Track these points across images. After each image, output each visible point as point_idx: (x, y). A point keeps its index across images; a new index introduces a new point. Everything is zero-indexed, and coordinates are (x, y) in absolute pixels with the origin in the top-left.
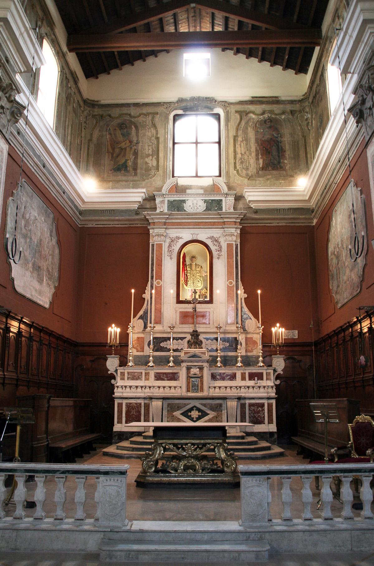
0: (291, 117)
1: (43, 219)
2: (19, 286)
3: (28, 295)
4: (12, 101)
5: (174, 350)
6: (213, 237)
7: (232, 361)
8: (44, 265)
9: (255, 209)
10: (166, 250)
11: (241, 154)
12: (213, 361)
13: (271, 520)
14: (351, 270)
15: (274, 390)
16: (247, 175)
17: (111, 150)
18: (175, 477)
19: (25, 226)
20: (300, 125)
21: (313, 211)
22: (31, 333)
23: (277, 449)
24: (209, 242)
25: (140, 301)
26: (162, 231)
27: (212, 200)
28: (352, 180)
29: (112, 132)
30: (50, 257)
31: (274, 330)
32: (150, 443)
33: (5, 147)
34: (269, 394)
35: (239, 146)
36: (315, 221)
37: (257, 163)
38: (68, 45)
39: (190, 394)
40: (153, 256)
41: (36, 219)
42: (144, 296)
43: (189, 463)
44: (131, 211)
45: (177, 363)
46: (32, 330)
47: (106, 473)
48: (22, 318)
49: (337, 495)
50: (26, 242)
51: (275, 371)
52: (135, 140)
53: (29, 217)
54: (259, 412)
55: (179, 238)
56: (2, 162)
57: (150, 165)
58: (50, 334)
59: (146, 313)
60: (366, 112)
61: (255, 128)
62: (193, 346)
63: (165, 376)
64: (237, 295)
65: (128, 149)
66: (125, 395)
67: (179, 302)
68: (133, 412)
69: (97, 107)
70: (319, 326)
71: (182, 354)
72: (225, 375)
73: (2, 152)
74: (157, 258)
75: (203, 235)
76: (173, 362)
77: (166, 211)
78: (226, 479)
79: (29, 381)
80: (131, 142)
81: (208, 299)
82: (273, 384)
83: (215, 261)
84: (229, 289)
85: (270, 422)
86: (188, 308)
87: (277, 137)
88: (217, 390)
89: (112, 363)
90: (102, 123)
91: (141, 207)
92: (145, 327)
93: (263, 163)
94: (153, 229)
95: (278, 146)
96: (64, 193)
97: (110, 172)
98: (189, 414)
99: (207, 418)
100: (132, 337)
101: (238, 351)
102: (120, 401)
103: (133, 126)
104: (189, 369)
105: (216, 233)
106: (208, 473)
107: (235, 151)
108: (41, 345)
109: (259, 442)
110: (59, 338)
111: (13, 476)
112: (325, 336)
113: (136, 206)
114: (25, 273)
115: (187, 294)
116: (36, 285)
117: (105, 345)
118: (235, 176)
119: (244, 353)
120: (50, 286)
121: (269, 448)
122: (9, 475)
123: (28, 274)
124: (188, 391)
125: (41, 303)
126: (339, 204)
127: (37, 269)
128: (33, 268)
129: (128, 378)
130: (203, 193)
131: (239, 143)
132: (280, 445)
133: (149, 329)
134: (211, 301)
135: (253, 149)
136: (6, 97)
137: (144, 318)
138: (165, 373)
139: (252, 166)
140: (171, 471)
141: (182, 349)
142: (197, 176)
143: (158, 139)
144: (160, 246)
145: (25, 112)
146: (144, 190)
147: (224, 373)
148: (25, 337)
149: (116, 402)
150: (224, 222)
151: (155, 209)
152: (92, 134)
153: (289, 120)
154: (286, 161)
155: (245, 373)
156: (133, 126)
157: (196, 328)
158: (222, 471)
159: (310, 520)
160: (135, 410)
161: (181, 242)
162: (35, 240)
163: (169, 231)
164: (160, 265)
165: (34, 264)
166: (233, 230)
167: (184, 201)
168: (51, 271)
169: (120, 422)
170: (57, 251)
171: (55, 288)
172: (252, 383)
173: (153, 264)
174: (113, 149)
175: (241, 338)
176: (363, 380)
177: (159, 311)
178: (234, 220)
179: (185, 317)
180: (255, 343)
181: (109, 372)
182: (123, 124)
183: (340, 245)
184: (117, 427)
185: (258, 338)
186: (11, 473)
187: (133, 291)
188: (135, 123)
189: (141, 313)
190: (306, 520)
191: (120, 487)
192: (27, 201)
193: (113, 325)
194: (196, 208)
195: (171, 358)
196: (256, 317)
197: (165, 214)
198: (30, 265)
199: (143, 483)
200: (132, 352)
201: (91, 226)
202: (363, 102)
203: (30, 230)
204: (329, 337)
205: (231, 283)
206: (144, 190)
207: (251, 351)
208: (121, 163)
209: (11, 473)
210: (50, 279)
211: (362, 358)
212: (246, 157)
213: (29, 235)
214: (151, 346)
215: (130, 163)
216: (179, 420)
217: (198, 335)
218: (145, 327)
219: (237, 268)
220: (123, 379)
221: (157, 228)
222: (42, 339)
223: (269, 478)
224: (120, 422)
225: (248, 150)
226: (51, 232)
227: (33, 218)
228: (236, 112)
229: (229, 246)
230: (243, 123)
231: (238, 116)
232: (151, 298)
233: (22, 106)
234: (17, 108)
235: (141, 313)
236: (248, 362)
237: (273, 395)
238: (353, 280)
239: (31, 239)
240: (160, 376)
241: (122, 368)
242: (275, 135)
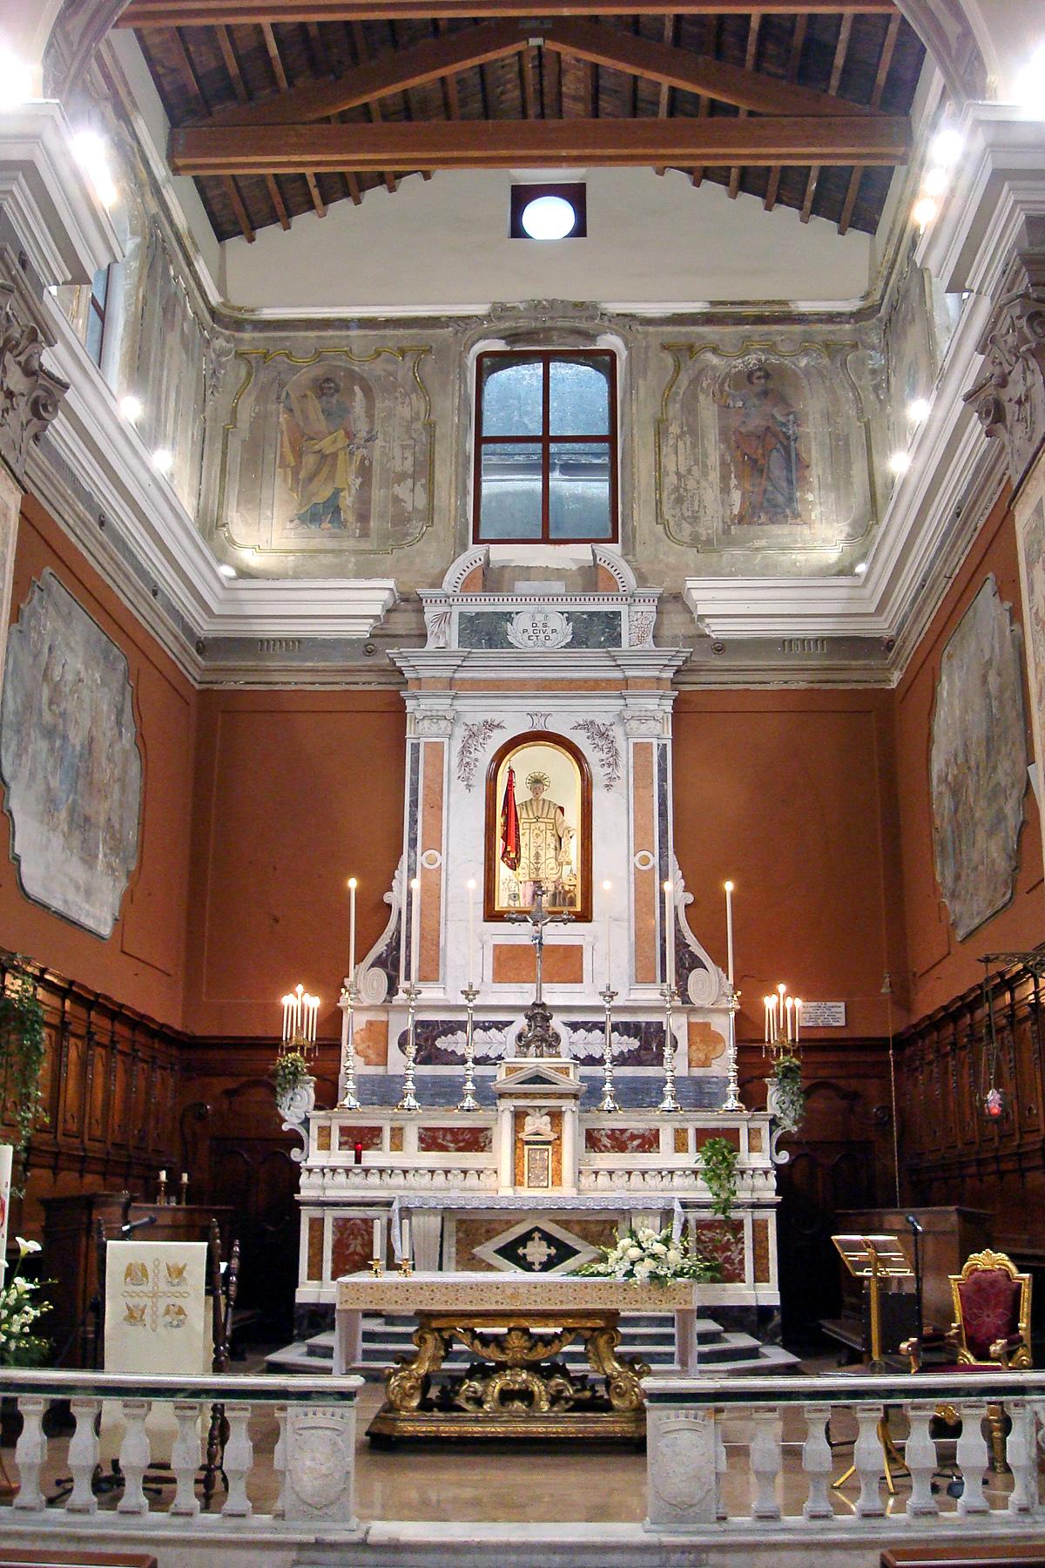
0: (826, 361)
1: (97, 676)
2: (34, 878)
3: (56, 904)
4: (32, 372)
5: (477, 1061)
6: (592, 722)
7: (648, 1092)
8: (101, 810)
9: (718, 641)
10: (455, 761)
11: (678, 473)
12: (590, 1095)
13: (724, 1518)
14: (991, 834)
15: (773, 1182)
17: (291, 459)
18: (477, 1420)
19: (51, 703)
20: (854, 387)
21: (890, 645)
22: (64, 1012)
23: (778, 1355)
24: (580, 739)
25: (377, 912)
26: (441, 705)
27: (591, 614)
28: (990, 575)
29: (296, 406)
30: (117, 787)
31: (770, 1002)
32: (405, 1338)
33: (14, 500)
34: (756, 1195)
35: (670, 450)
36: (896, 677)
38: (171, 156)
39: (13, 1395)
40: (416, 776)
41: (81, 680)
42: (387, 897)
43: (515, 1382)
44: (350, 642)
45: (486, 1098)
46: (68, 1003)
47: (304, 1395)
48: (43, 971)
49: (895, 1454)
50: (52, 750)
51: (774, 1122)
52: (362, 428)
53: (62, 676)
55: (491, 726)
56: (5, 544)
58: (116, 1013)
59: (394, 947)
60: (1011, 410)
61: (720, 397)
62: (532, 1049)
63: (449, 1137)
64: (662, 894)
65: (341, 456)
66: (332, 1194)
67: (492, 915)
68: (356, 1245)
69: (248, 327)
70: (908, 991)
71: (500, 1073)
72: (627, 1134)
73: (5, 516)
74: (426, 787)
76: (476, 1096)
77: (455, 646)
78: (618, 1428)
79: (57, 1154)
80: (350, 435)
82: (768, 1164)
83: (598, 795)
84: (641, 882)
85: (761, 1276)
86: (521, 934)
87: (784, 424)
88: (603, 1180)
89: (296, 1107)
90: (264, 377)
91: (382, 635)
92: (392, 990)
93: (742, 503)
94: (416, 697)
95: (787, 449)
96: (155, 593)
97: (289, 525)
98: (521, 1251)
99: (571, 1263)
100: (354, 1024)
101: (667, 1066)
103: (357, 388)
104: (519, 1116)
105: (602, 710)
106: (568, 1411)
107: (659, 465)
108: (89, 1047)
109: (725, 1335)
110: (138, 1022)
111: (66, 1403)
112: (923, 1020)
113: (363, 629)
114: (49, 840)
116: (78, 871)
117: (273, 1045)
118: (659, 540)
119: (682, 1070)
120: (113, 870)
121: (752, 1353)
122: (53, 1401)
123: (57, 841)
124: (516, 1181)
125: (89, 923)
126: (957, 637)
127: (81, 823)
128: (71, 822)
129: (341, 1144)
130: (563, 591)
131: (671, 442)
132: (788, 1346)
133: (401, 996)
134: (585, 916)
135: (714, 459)
136: (19, 363)
137: (390, 964)
138: (451, 1130)
140: (465, 1406)
141: (500, 1058)
142: (546, 540)
143: (430, 427)
144: (436, 750)
145: (69, 395)
146: (390, 583)
147: (623, 1131)
148: (47, 1024)
149: (306, 1215)
150: (626, 679)
151: (423, 637)
152: (234, 411)
153: (820, 373)
154: (810, 497)
155: (685, 1130)
156: (357, 388)
157: (540, 1008)
158: (607, 1407)
159: (825, 1517)
160: (359, 1241)
161: (499, 739)
162: (76, 739)
163: (460, 705)
164: (436, 806)
165: (72, 811)
166: (651, 704)
167: (508, 617)
168: (117, 826)
170: (135, 768)
171: (129, 875)
172: (433, 1159)
173: (414, 804)
174: (299, 455)
175: (677, 1025)
176: (1020, 1155)
177: (432, 942)
178: (656, 674)
180: (716, 1039)
181: (285, 1127)
182: (328, 380)
183: (960, 759)
184: (307, 1292)
185: (724, 1026)
186: (60, 1397)
187: (353, 883)
188: (362, 379)
189: (380, 947)
190: (814, 1517)
191: (339, 1432)
192: (56, 631)
193: (300, 988)
194: (542, 636)
195: (470, 1086)
196: (720, 961)
197: (452, 655)
198: (63, 815)
199: (389, 1437)
200: (353, 1065)
201: (231, 686)
202: (1003, 383)
203: (63, 714)
204: (934, 1023)
205: (645, 861)
206: (390, 583)
207: (705, 1064)
208: (320, 499)
209: (60, 1397)
210: (114, 850)
211: (993, 1097)
212: (691, 484)
213: (61, 727)
214: (412, 1049)
215: (347, 500)
216: (490, 1268)
217: (547, 1019)
218: (392, 990)
219: (663, 815)
221: (428, 697)
222: (68, 1018)
223: (719, 1410)
224: (315, 1274)
225: (696, 463)
226: (120, 712)
227: (70, 677)
228: (664, 347)
229: (641, 750)
230: (684, 380)
231: (669, 360)
232: (409, 904)
233: (58, 381)
234: (47, 390)
235: (380, 947)
236: (699, 1094)
237: (770, 1195)
238: (993, 862)
239: (65, 738)
240: (434, 1138)
241: (322, 1113)
242: (780, 418)
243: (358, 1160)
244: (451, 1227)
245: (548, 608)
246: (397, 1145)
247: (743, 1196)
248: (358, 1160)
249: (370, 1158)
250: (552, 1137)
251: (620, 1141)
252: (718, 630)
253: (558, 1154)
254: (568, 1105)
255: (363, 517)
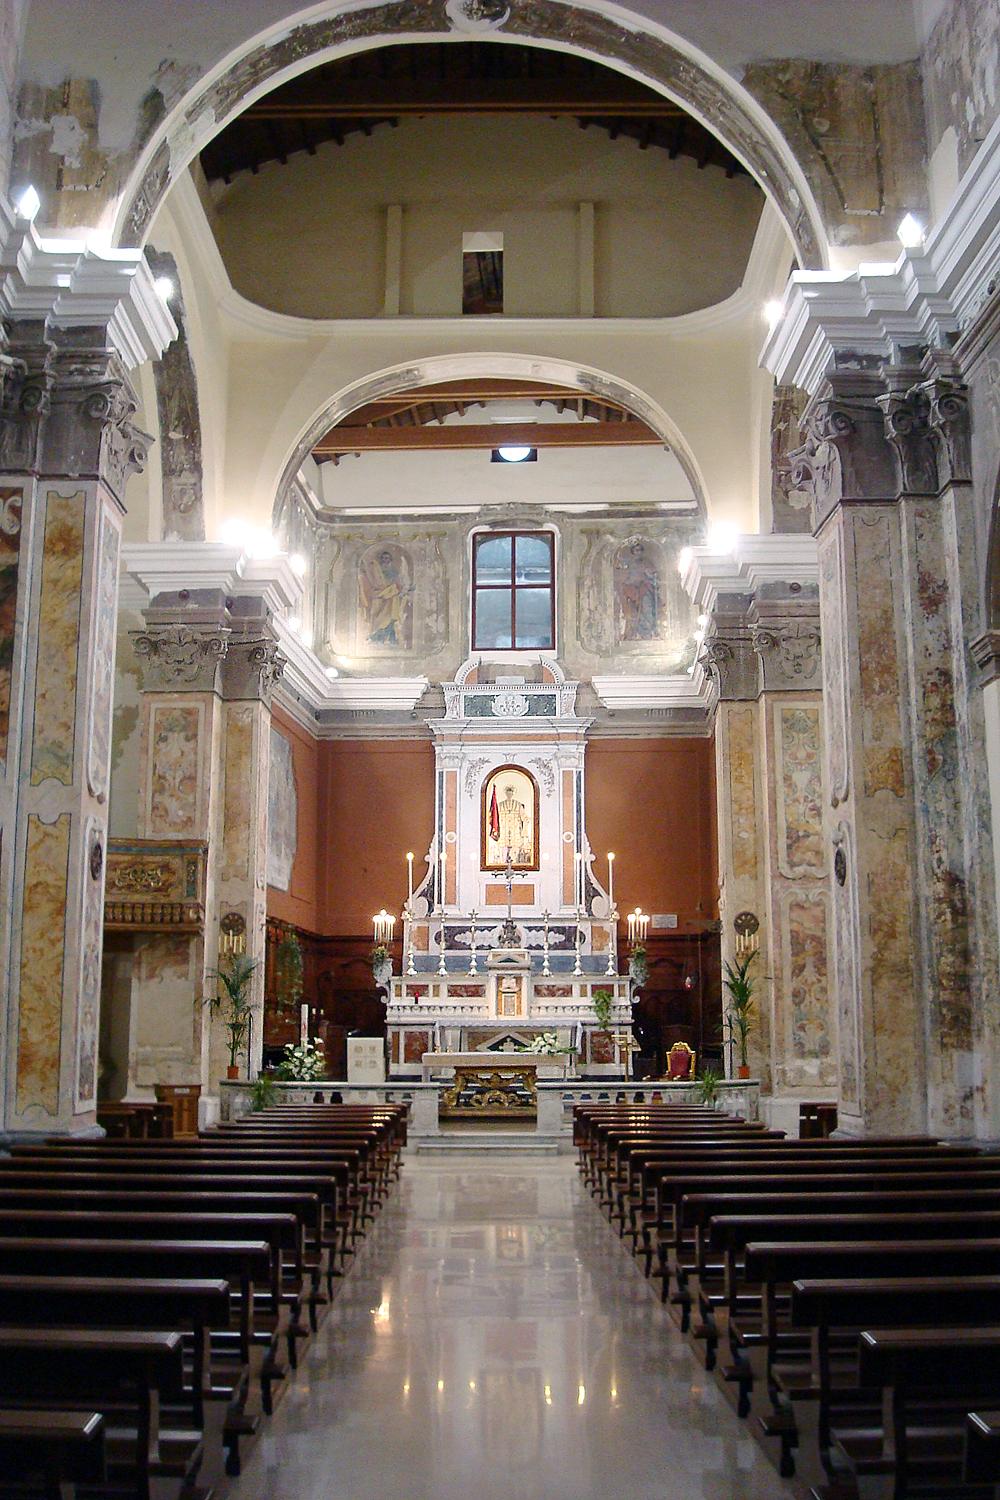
16: (599, 648)
24: (532, 768)
25: (422, 866)
26: (455, 749)
31: (631, 919)
37: (617, 628)
42: (427, 858)
54: (606, 1046)
55: (484, 761)
57: (434, 630)
65: (394, 600)
66: (403, 1020)
68: (416, 1046)
75: (523, 755)
81: (532, 864)
88: (543, 1011)
89: (383, 975)
90: (348, 551)
91: (421, 708)
95: (653, 595)
102: (396, 1029)
104: (499, 979)
105: (545, 751)
111: (339, 1094)
113: (409, 705)
115: (496, 853)
134: (535, 868)
135: (610, 601)
137: (428, 894)
139: (608, 633)
143: (446, 582)
144: (453, 776)
154: (665, 623)
156: (403, 558)
161: (488, 768)
164: (453, 807)
166: (573, 748)
167: (492, 698)
169: (180, 1129)
173: (441, 806)
174: (370, 600)
179: (493, 895)
181: (378, 985)
185: (611, 927)
189: (424, 886)
197: (462, 722)
200: (410, 950)
201: (336, 738)
205: (569, 837)
215: (399, 627)
218: (431, 909)
220: (399, 995)
228: (582, 532)
230: (594, 552)
235: (424, 886)
237: (629, 1019)
240: (455, 992)
243: (416, 1002)
244: (465, 1035)
245: (515, 693)
246: (436, 994)
247: (615, 1019)
248: (416, 1002)
249: (423, 1001)
250: (516, 990)
251: (552, 992)
252: (611, 704)
253: (519, 998)
254: (524, 973)
255: (408, 637)
